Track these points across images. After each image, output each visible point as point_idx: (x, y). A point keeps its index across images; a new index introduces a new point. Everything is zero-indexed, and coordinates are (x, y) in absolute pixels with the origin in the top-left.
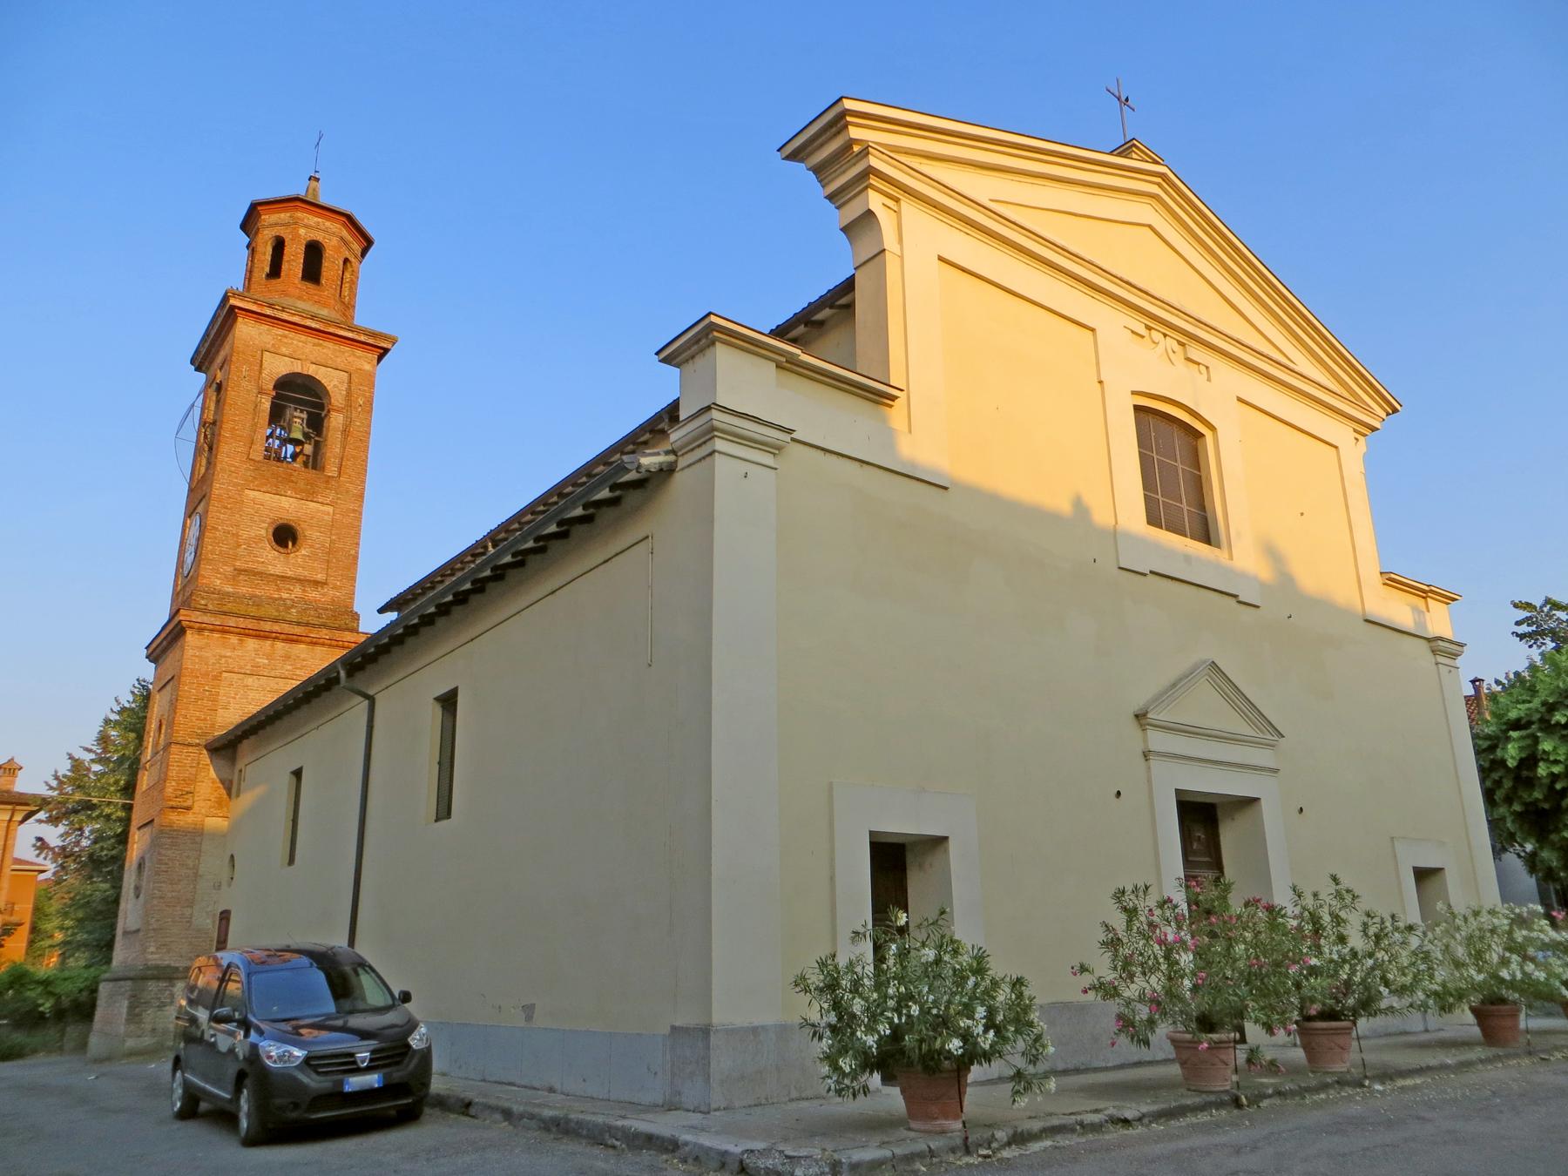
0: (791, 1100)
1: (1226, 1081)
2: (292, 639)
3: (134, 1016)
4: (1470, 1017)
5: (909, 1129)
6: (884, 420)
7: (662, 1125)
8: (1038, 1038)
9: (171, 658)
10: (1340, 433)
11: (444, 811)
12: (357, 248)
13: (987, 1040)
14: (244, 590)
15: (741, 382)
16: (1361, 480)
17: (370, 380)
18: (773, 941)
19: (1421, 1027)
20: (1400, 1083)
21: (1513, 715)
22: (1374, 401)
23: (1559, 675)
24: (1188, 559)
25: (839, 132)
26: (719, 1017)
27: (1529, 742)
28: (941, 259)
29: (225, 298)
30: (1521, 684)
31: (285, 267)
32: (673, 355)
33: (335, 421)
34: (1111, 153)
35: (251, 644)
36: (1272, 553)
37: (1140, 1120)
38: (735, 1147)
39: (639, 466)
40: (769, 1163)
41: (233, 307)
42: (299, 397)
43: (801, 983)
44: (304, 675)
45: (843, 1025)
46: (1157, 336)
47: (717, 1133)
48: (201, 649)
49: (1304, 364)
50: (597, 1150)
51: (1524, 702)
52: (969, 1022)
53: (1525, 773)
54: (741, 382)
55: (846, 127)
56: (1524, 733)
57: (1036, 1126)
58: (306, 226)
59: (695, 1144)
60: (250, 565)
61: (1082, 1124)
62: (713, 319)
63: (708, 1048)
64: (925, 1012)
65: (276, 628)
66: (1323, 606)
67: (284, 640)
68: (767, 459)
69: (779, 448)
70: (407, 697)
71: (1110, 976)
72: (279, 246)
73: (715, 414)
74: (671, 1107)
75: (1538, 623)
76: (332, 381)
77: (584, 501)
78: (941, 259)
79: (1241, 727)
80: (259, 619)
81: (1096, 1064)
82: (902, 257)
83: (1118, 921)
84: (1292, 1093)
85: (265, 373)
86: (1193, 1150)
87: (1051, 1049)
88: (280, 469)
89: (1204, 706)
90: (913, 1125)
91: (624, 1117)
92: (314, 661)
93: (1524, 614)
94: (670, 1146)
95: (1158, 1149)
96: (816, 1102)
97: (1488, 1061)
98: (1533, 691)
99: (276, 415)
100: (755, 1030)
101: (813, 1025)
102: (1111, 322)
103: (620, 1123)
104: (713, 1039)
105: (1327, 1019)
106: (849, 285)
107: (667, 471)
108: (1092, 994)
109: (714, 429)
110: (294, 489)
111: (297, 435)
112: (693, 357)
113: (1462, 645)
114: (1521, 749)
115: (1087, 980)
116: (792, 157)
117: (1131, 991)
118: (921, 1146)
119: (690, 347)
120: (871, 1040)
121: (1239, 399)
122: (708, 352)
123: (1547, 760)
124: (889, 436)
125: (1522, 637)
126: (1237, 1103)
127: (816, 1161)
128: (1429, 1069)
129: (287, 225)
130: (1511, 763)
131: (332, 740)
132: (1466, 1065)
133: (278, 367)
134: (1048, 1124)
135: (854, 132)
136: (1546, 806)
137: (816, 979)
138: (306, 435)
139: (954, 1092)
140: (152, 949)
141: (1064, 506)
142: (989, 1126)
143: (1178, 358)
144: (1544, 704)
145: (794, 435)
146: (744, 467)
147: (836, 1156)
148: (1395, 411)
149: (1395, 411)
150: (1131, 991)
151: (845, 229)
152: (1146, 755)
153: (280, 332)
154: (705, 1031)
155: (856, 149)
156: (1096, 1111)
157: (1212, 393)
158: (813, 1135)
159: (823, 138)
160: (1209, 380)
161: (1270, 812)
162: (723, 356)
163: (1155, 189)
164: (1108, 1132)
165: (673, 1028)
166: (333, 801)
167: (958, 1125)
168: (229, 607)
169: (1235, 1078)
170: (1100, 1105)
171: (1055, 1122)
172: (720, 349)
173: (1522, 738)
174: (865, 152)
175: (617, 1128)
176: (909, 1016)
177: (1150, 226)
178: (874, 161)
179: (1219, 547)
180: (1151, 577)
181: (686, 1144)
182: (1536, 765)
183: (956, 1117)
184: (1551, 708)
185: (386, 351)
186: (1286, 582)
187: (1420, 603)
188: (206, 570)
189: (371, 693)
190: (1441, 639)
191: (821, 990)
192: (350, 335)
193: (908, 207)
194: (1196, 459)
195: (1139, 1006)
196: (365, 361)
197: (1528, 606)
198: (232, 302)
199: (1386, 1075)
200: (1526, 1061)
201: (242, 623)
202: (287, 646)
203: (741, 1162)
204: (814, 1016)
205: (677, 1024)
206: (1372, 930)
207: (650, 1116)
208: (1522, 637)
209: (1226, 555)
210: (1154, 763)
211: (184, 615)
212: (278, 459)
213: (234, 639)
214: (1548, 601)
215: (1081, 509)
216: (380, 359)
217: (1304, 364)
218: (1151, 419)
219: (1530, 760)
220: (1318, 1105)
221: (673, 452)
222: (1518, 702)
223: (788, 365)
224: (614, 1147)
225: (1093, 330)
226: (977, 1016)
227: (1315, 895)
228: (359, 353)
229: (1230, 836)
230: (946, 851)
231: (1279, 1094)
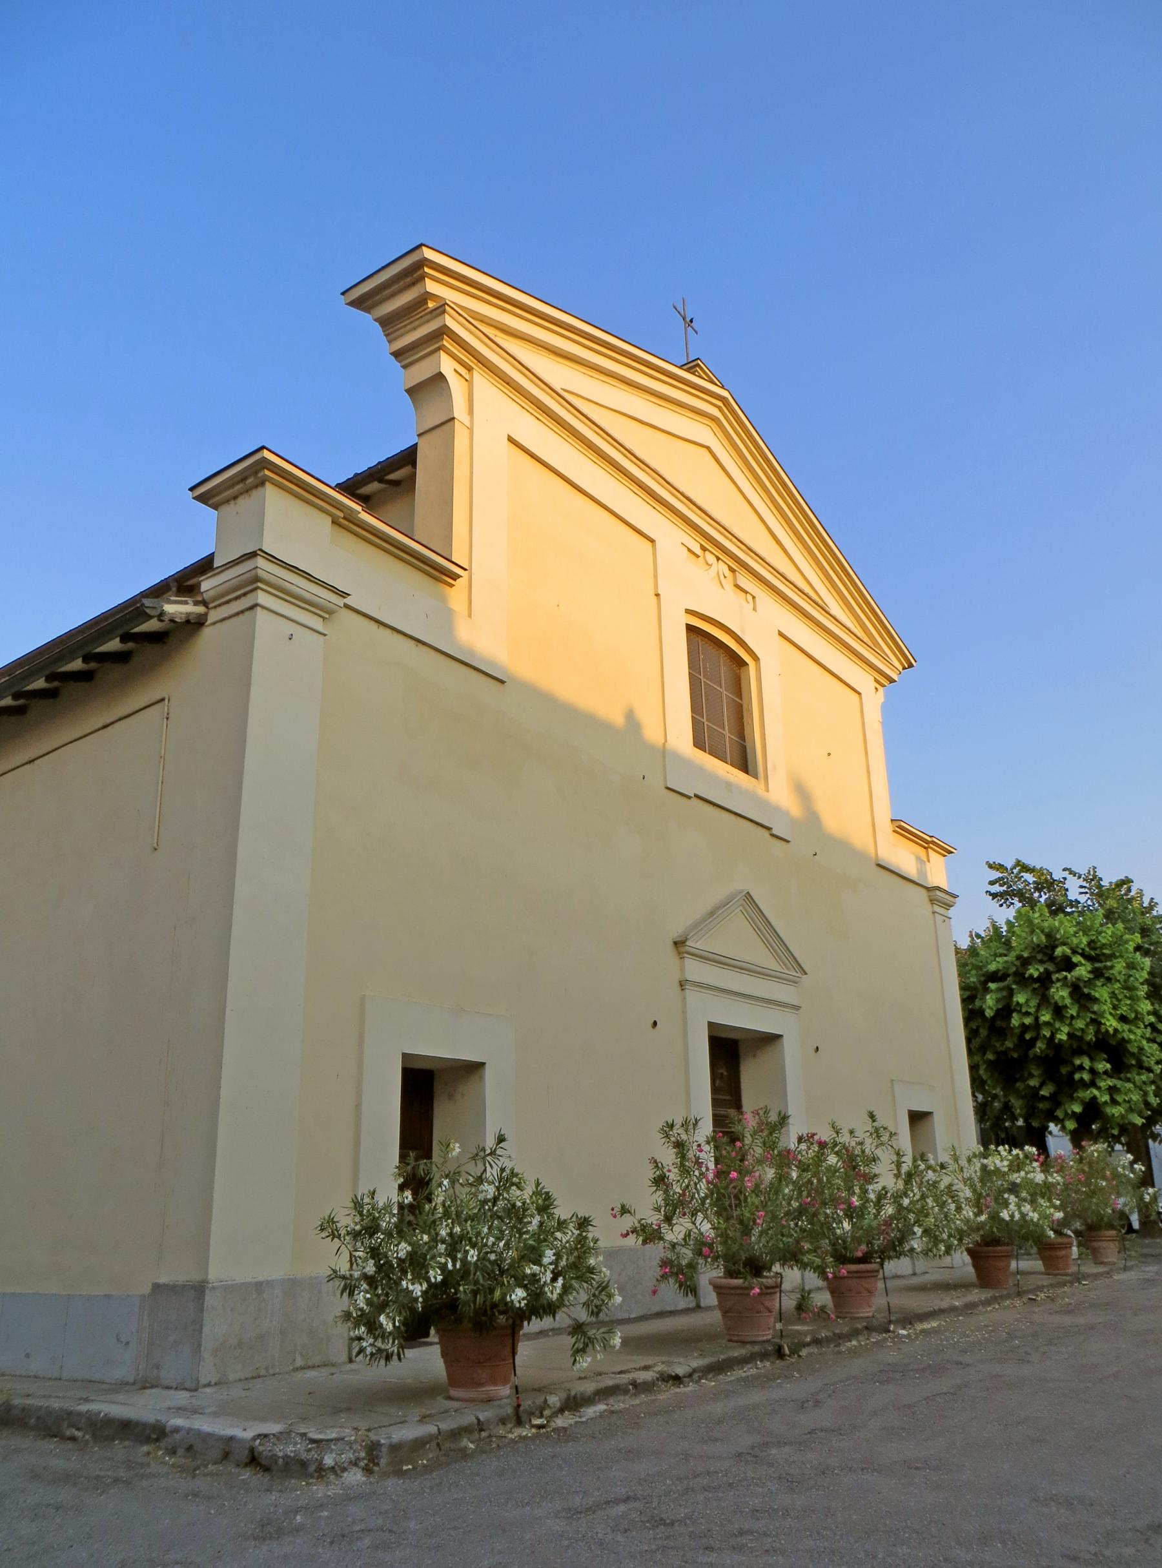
0: (296, 1370)
1: (767, 1331)
4: (967, 1259)
5: (450, 1398)
6: (443, 600)
7: (141, 1408)
8: (604, 1287)
10: (863, 679)
13: (553, 1292)
15: (290, 530)
16: (878, 728)
18: (284, 1202)
19: (910, 1271)
20: (919, 1327)
21: (992, 967)
22: (896, 656)
23: (1032, 932)
24: (729, 785)
25: (414, 284)
26: (217, 1272)
27: (1005, 993)
28: (511, 440)
30: (998, 938)
32: (211, 494)
34: (681, 367)
36: (801, 791)
37: (690, 1375)
38: (244, 1432)
39: (162, 613)
40: (290, 1450)
43: (329, 1227)
45: (385, 1275)
46: (711, 558)
47: (216, 1415)
49: (836, 608)
50: (51, 1445)
51: (1001, 955)
52: (536, 1268)
53: (999, 1023)
54: (290, 530)
55: (422, 278)
56: (1000, 985)
57: (589, 1387)
59: (189, 1430)
61: (634, 1384)
62: (266, 454)
63: (202, 1310)
64: (482, 1258)
66: (841, 846)
68: (317, 623)
69: (330, 612)
71: (654, 1219)
73: (261, 562)
74: (145, 1384)
75: (1010, 884)
77: (47, 672)
78: (511, 440)
79: (768, 961)
82: (471, 429)
83: (668, 1157)
84: (828, 1340)
87: (618, 1299)
89: (736, 938)
90: (454, 1392)
91: (87, 1400)
93: (996, 875)
94: (155, 1434)
95: (718, 1408)
96: (325, 1371)
97: (988, 1302)
98: (1007, 943)
100: (259, 1287)
101: (344, 1277)
102: (671, 538)
103: (84, 1408)
104: (209, 1299)
105: (856, 1261)
106: (409, 457)
107: (194, 625)
108: (632, 1238)
109: (257, 579)
112: (235, 498)
113: (956, 896)
114: (998, 1000)
115: (628, 1222)
116: (358, 303)
117: (676, 1232)
118: (468, 1419)
119: (234, 485)
120: (417, 1289)
121: (781, 634)
122: (255, 494)
123: (1019, 1012)
124: (448, 615)
125: (994, 896)
126: (779, 1353)
127: (350, 1443)
128: (942, 1311)
130: (989, 1013)
132: (970, 1307)
134: (602, 1385)
135: (431, 287)
136: (1015, 1055)
137: (347, 1221)
139: (509, 1349)
141: (618, 718)
142: (539, 1390)
143: (728, 584)
144: (1019, 957)
145: (348, 601)
147: (373, 1436)
148: (911, 666)
149: (911, 666)
150: (676, 1232)
151: (411, 391)
152: (682, 985)
154: (199, 1289)
155: (431, 305)
156: (646, 1368)
157: (758, 623)
158: (337, 1411)
159: (395, 287)
160: (755, 609)
161: (791, 1051)
163: (715, 412)
164: (659, 1392)
165: (157, 1287)
167: (505, 1391)
169: (779, 1326)
170: (648, 1361)
171: (610, 1382)
172: (269, 490)
173: (1000, 989)
174: (441, 309)
175: (80, 1414)
176: (464, 1261)
177: (708, 448)
178: (450, 322)
179: (756, 777)
180: (695, 800)
181: (177, 1430)
182: (1009, 1017)
183: (505, 1381)
184: (1025, 962)
186: (812, 818)
187: (922, 852)
190: (938, 888)
191: (356, 1235)
193: (480, 379)
194: (738, 687)
195: (684, 1250)
197: (1000, 867)
199: (908, 1320)
200: (1018, 1302)
203: (252, 1450)
204: (344, 1267)
205: (162, 1280)
206: (905, 1168)
207: (121, 1397)
208: (994, 896)
209: (763, 787)
210: (692, 994)
214: (1018, 863)
215: (632, 722)
217: (836, 608)
218: (699, 639)
219: (1006, 1010)
220: (853, 1353)
221: (204, 603)
222: (996, 955)
223: (346, 523)
224: (73, 1439)
226: (546, 1261)
227: (851, 1132)
229: (751, 1076)
230: (482, 1078)
231: (816, 1342)
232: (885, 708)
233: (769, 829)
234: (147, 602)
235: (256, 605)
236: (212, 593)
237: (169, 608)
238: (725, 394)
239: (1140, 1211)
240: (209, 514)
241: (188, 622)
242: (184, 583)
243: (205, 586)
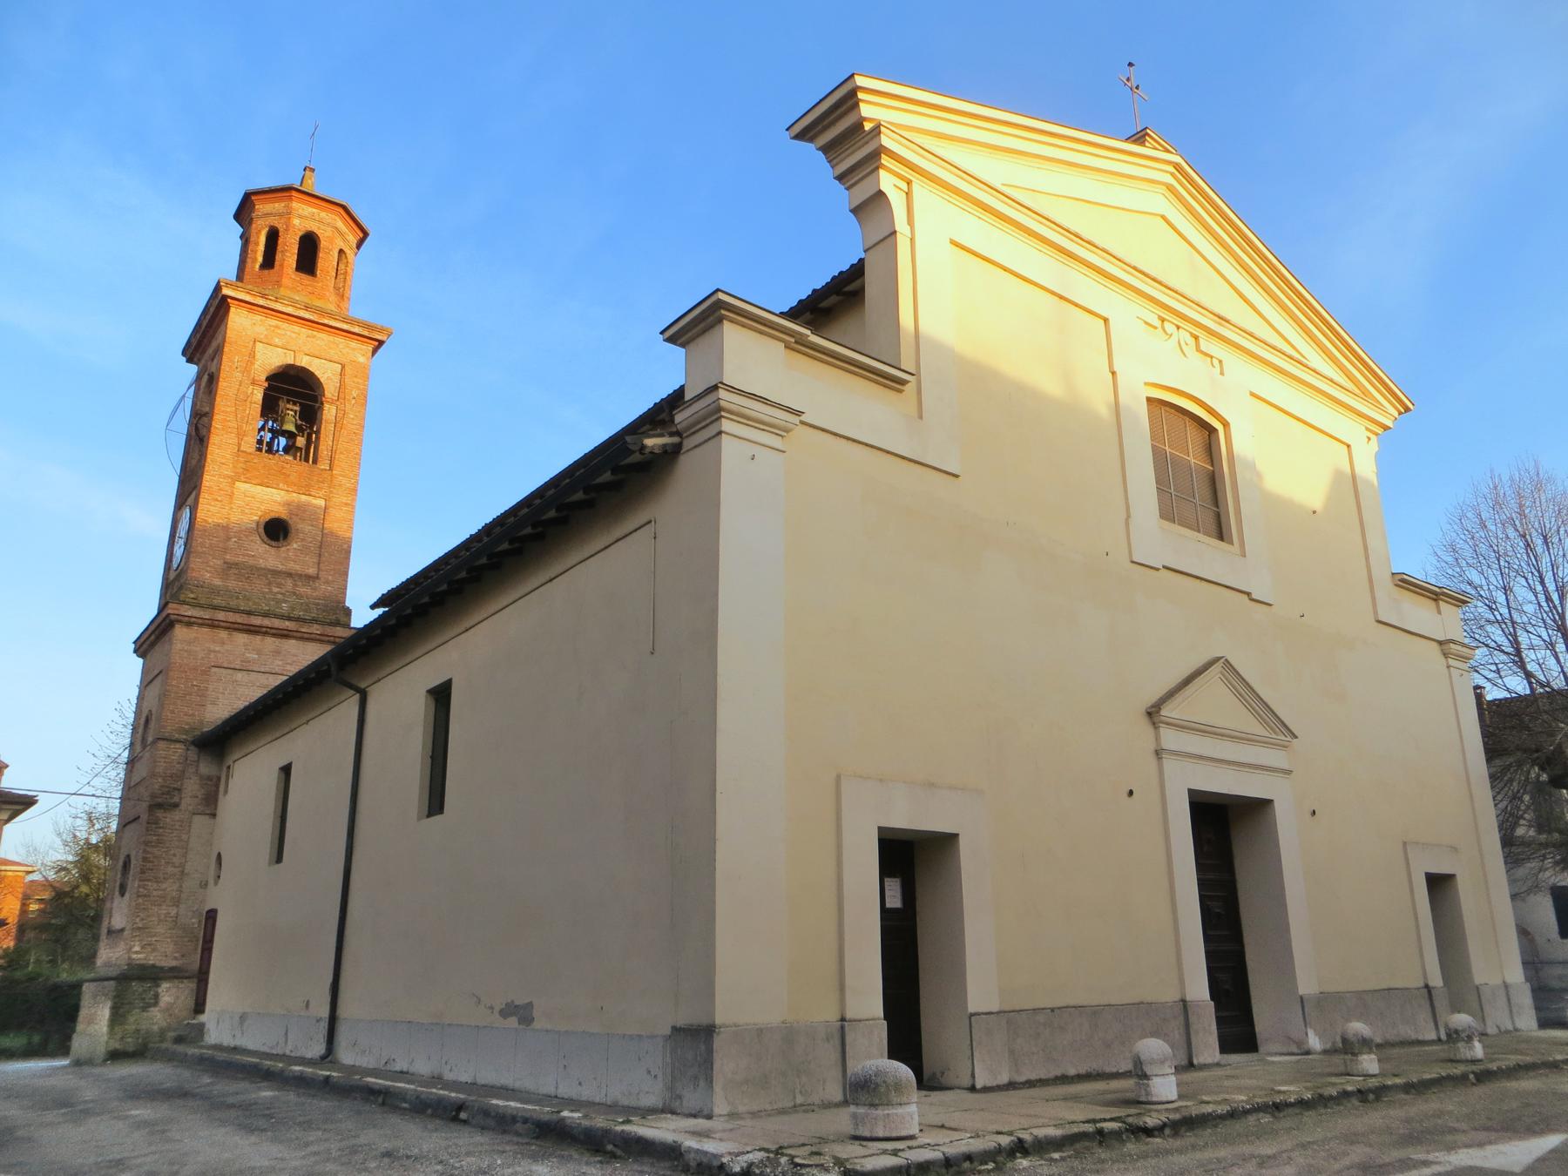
2: (284, 635)
3: (117, 1017)
9: (157, 654)
11: (435, 802)
12: (353, 239)
14: (232, 584)
17: (364, 372)
18: (787, 942)
26: (718, 1021)
29: (218, 288)
31: (278, 257)
33: (329, 412)
35: (241, 638)
39: (643, 447)
41: (225, 297)
42: (293, 393)
44: (293, 670)
46: (1170, 328)
48: (189, 643)
54: (751, 362)
58: (300, 217)
60: (241, 559)
61: (1100, 1132)
62: (721, 296)
65: (267, 622)
67: (274, 635)
70: (399, 695)
72: (273, 236)
76: (325, 372)
79: (1254, 727)
80: (249, 613)
81: (1108, 1069)
85: (257, 364)
86: (1219, 1161)
88: (271, 461)
92: (303, 655)
99: (269, 407)
100: (760, 1032)
101: (87, 1113)
102: (1126, 313)
103: (619, 1128)
104: (718, 1042)
106: (858, 270)
109: (720, 409)
110: (286, 483)
111: (290, 427)
119: (696, 326)
121: (1252, 394)
122: (716, 330)
129: (281, 215)
131: (319, 739)
133: (271, 359)
138: (298, 427)
140: (137, 948)
143: (1190, 349)
145: (803, 418)
146: (757, 450)
148: (1407, 410)
151: (855, 211)
152: (1158, 753)
153: (274, 322)
160: (1222, 373)
162: (732, 336)
166: (316, 799)
168: (218, 601)
177: (1164, 217)
179: (1231, 543)
185: (381, 343)
188: (195, 562)
189: (362, 685)
192: (345, 327)
193: (921, 189)
196: (358, 352)
198: (226, 291)
201: (232, 617)
202: (277, 641)
211: (172, 609)
212: (270, 451)
213: (223, 634)
216: (375, 351)
217: (1316, 360)
221: (678, 434)
223: (799, 346)
225: (1106, 320)
228: (354, 344)
232: (1379, 457)
233: (1249, 594)
234: (628, 439)
235: (720, 433)
236: (684, 424)
237: (649, 442)
238: (1178, 159)
239: (1048, 1152)
240: (678, 353)
241: (665, 452)
242: (661, 415)
243: (678, 418)
